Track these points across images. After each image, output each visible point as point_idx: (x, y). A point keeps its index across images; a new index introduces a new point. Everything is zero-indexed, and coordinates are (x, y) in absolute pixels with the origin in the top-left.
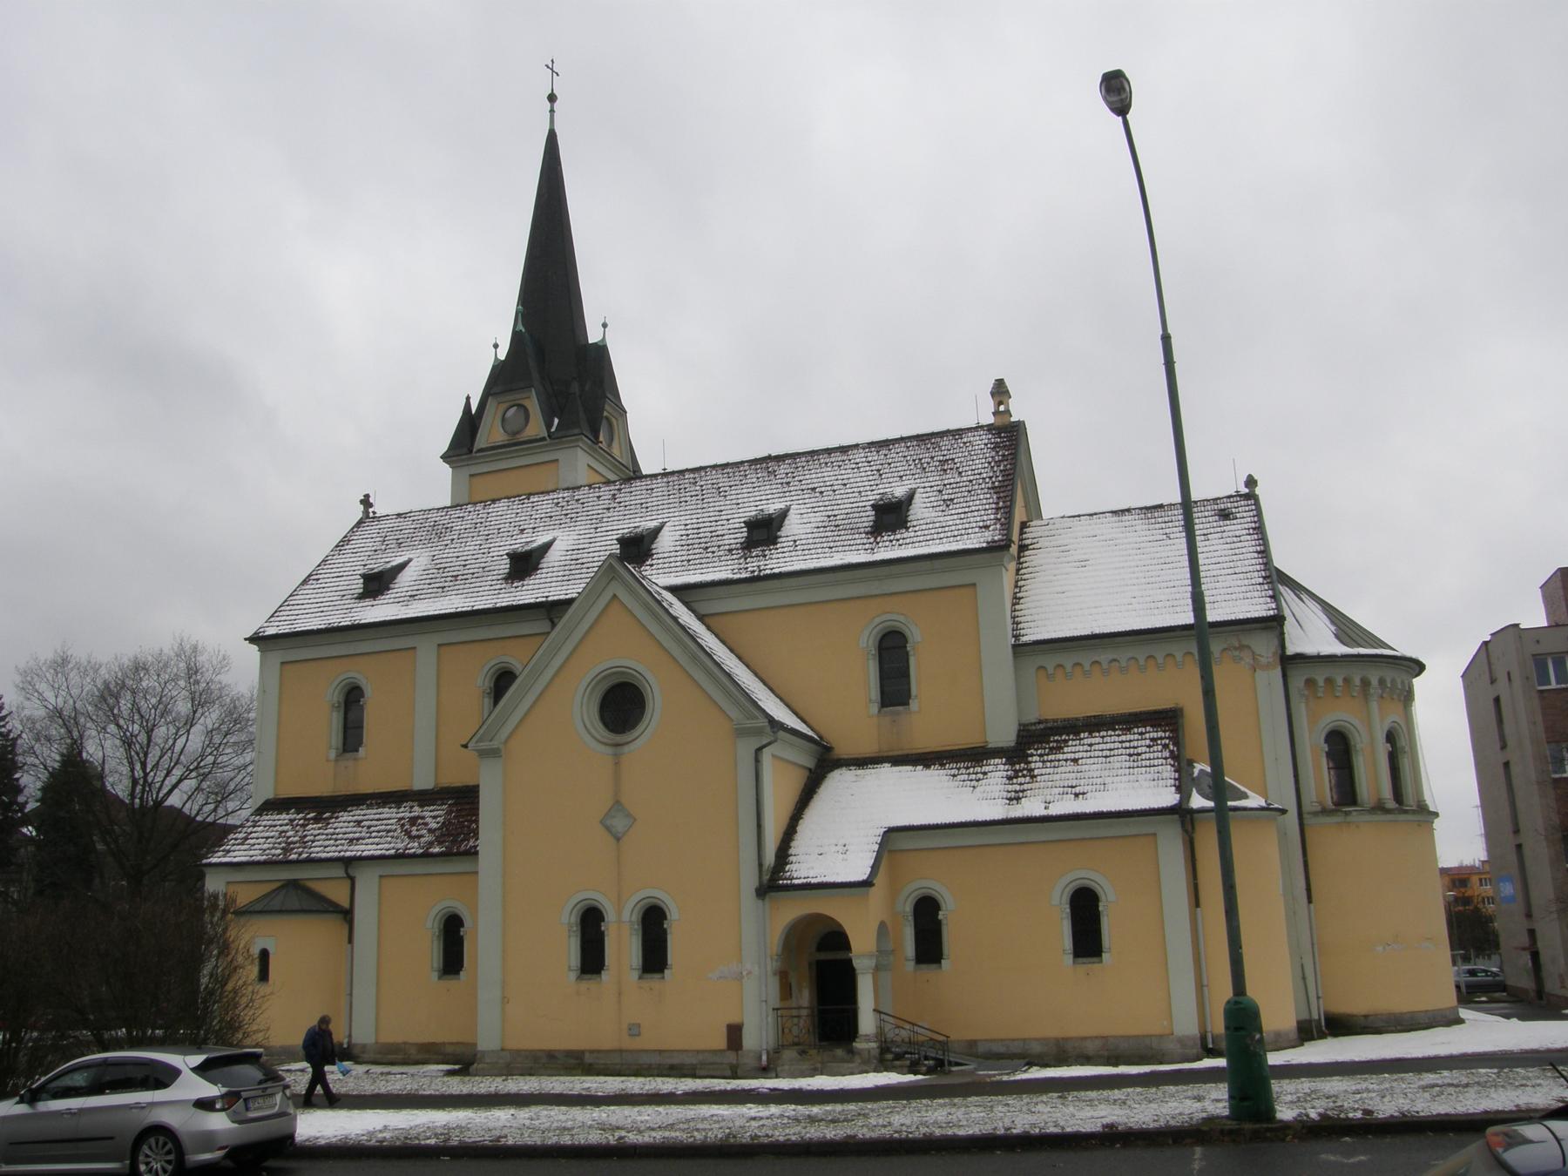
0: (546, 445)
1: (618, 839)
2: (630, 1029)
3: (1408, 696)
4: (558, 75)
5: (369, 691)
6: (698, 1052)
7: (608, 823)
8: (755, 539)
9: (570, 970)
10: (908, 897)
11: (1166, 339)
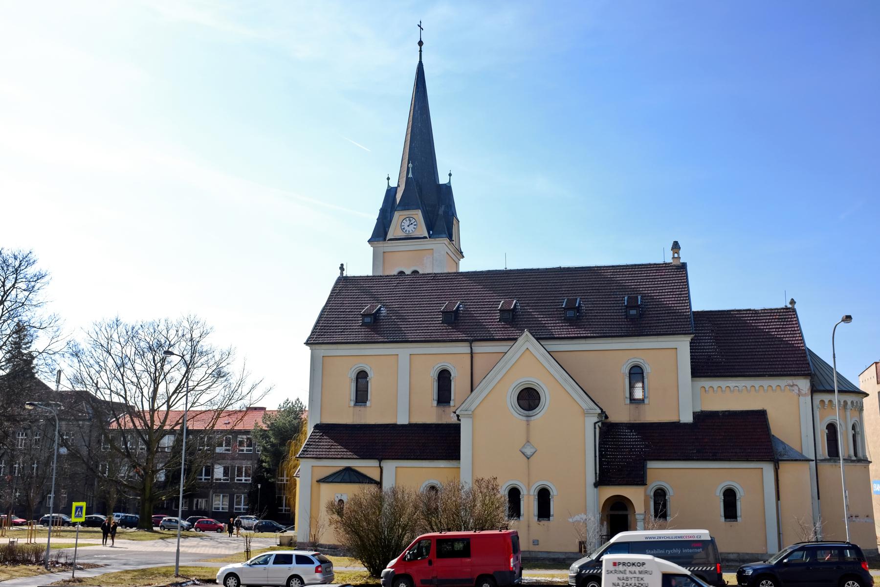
1: (528, 458)
2: (534, 542)
3: (861, 409)
4: (423, 30)
6: (566, 553)
7: (524, 450)
11: (834, 354)
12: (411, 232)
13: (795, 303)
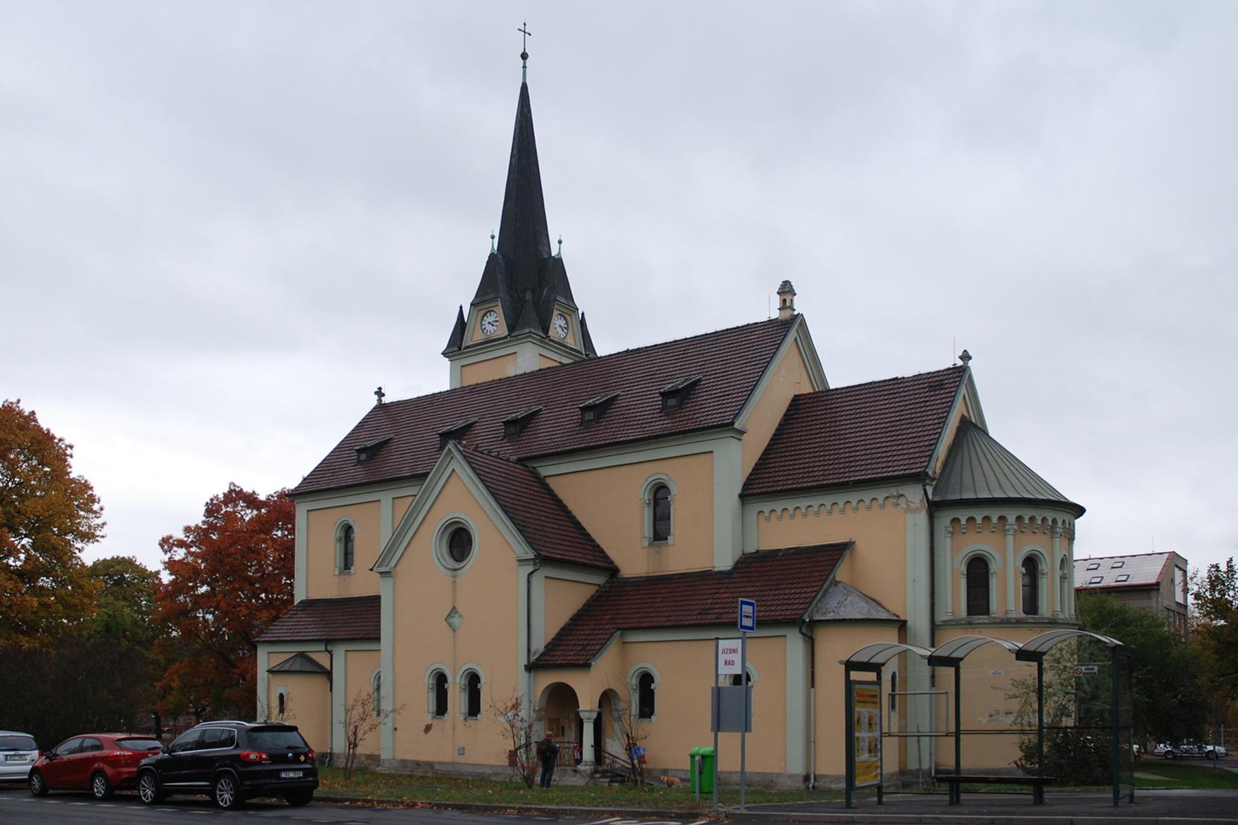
0: (507, 342)
4: (530, 34)
5: (674, 489)
6: (493, 766)
7: (450, 620)
8: (586, 419)
9: (429, 712)
10: (634, 674)
12: (492, 332)
13: (970, 358)
